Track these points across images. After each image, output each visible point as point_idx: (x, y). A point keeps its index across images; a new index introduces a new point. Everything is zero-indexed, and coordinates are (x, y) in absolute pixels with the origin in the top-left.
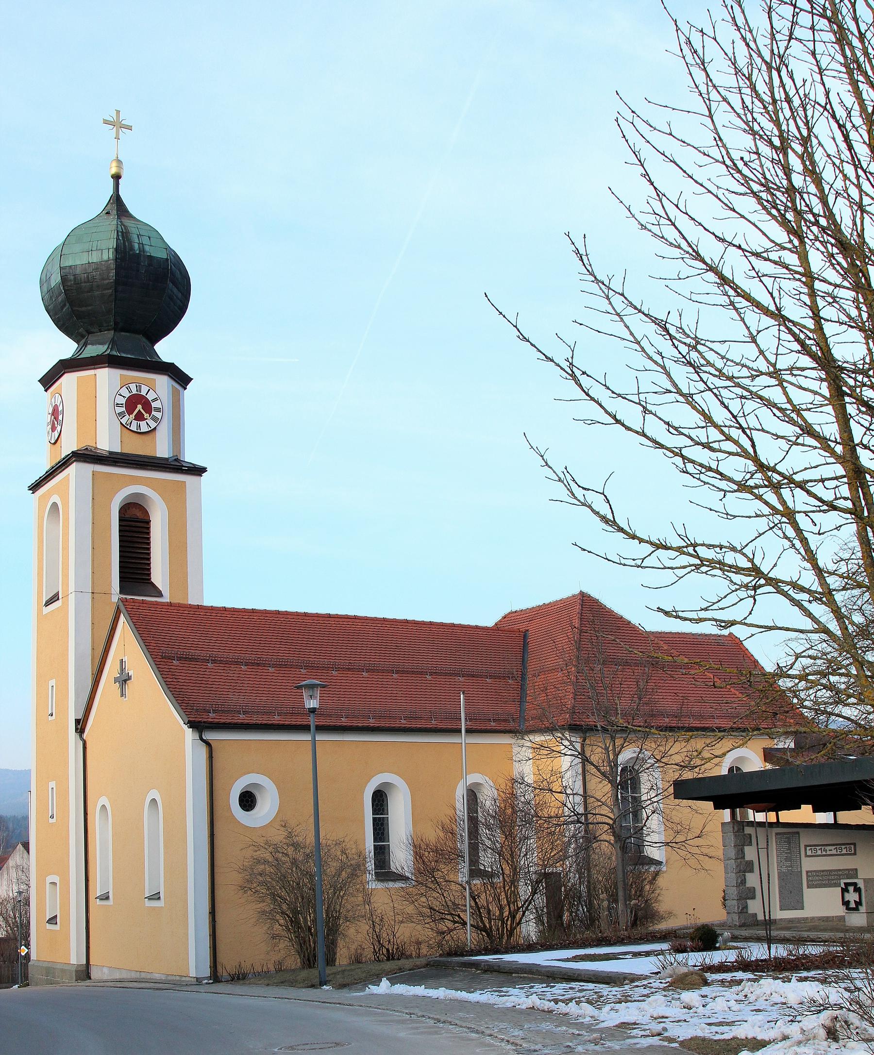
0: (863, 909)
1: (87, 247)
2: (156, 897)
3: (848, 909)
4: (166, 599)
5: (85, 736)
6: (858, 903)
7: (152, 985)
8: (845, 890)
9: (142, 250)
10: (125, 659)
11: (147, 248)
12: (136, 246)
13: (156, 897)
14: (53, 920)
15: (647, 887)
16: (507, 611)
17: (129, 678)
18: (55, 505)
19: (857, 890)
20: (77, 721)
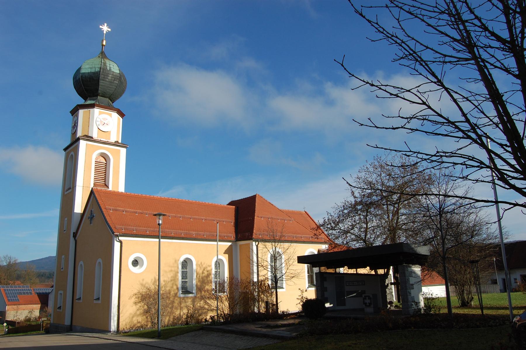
0: (372, 306)
1: (90, 66)
2: (98, 299)
3: (366, 306)
4: (111, 188)
5: (76, 238)
6: (370, 304)
7: (428, 69)
8: (365, 298)
9: (110, 70)
10: (93, 210)
11: (112, 69)
12: (108, 68)
13: (98, 299)
14: (60, 308)
15: (123, 231)
16: (231, 201)
17: (93, 216)
18: (72, 155)
19: (370, 298)
20: (74, 233)
